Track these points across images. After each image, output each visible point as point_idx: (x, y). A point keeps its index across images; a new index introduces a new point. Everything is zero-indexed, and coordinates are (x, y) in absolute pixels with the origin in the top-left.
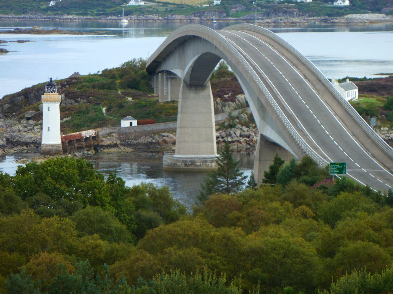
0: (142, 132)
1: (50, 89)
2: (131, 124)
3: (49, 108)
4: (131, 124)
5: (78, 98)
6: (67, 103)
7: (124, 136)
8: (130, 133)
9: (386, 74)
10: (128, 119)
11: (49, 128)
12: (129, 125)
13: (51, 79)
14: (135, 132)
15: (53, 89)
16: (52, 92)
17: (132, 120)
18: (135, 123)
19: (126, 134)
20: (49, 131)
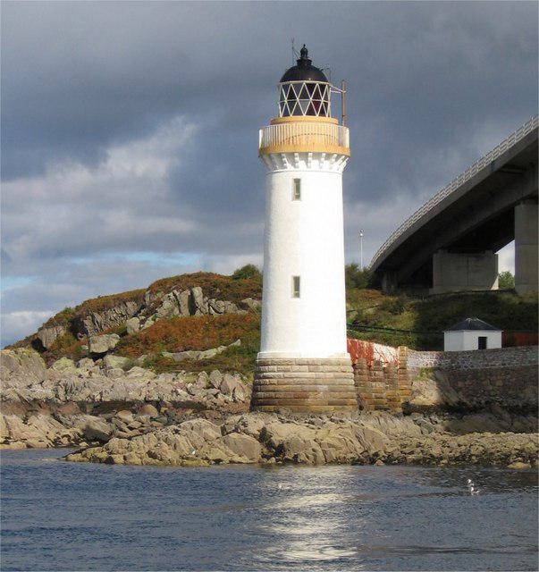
0: (527, 369)
1: (304, 96)
2: (482, 341)
3: (297, 182)
4: (482, 341)
5: (246, 296)
6: (213, 311)
7: (468, 382)
8: (489, 373)
9: (411, 547)
10: (472, 327)
11: (297, 280)
12: (476, 347)
13: (304, 52)
14: (506, 371)
15: (317, 96)
16: (311, 113)
17: (487, 329)
18: (495, 339)
19: (475, 375)
20: (297, 295)
